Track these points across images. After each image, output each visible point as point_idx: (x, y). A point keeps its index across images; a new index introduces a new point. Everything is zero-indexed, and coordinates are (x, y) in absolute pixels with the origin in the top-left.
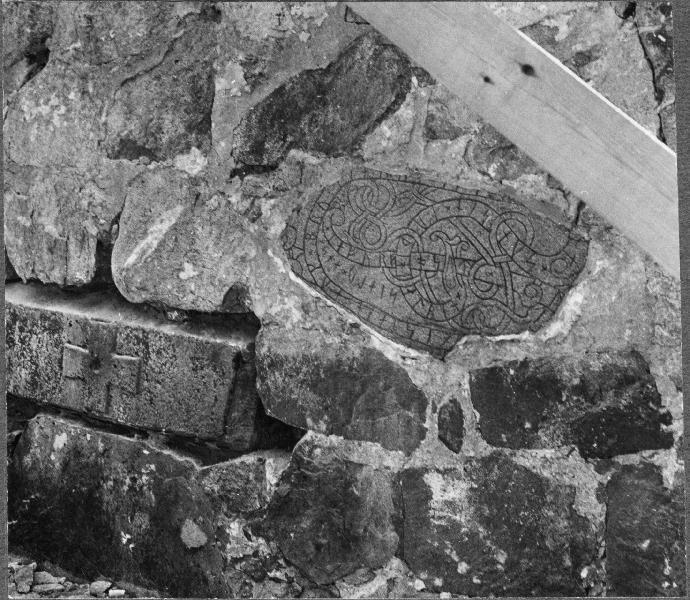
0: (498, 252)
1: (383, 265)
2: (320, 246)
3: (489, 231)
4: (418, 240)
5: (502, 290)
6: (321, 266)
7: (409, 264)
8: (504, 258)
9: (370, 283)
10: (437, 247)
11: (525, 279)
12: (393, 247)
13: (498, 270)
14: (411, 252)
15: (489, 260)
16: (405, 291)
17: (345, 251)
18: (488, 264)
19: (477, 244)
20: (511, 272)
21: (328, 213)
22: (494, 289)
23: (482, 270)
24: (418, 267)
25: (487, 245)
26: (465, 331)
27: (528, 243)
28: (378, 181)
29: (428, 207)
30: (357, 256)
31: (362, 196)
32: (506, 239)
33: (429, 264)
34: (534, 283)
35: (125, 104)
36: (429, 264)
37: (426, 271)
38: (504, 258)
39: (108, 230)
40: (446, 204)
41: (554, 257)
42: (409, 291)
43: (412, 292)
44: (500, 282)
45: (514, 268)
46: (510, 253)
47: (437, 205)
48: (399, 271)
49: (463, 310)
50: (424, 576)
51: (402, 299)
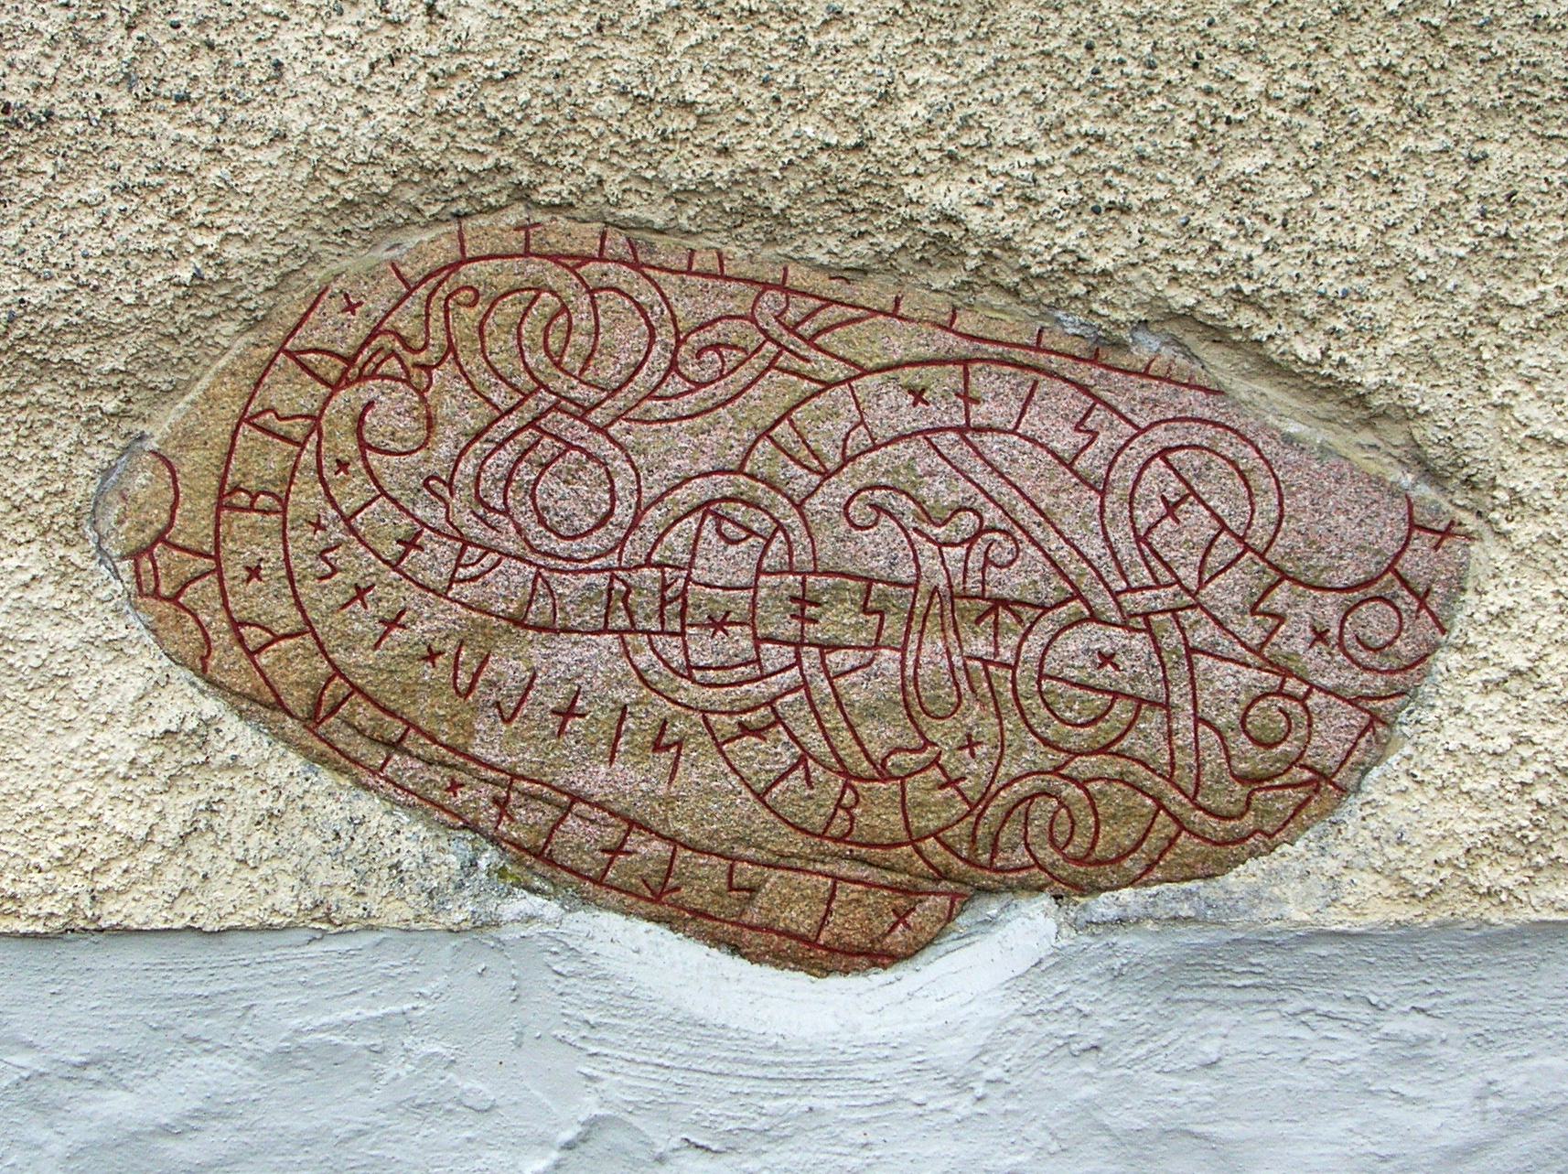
0: (1141, 575)
1: (621, 621)
3: (1103, 489)
4: (793, 520)
5: (1152, 721)
6: (308, 626)
7: (751, 621)
8: (1166, 596)
9: (558, 699)
10: (878, 548)
11: (1248, 675)
13: (1139, 643)
14: (760, 571)
15: (1102, 602)
16: (726, 724)
17: (434, 559)
18: (1094, 617)
19: (1054, 543)
20: (1191, 650)
23: (1074, 642)
24: (791, 629)
25: (1094, 548)
27: (1259, 539)
28: (592, 268)
29: (828, 385)
30: (497, 583)
33: (838, 620)
34: (1280, 692)
36: (838, 620)
38: (1166, 596)
39: (973, 407)
42: (745, 730)
43: (758, 732)
44: (1146, 689)
45: (1203, 634)
46: (1189, 576)
47: (872, 381)
48: (704, 647)
49: (987, 797)
51: (713, 763)
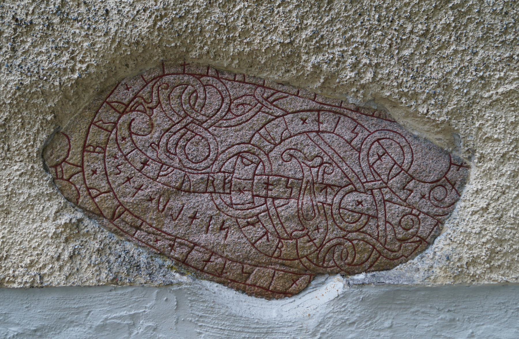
0: (370, 177)
2: (110, 162)
6: (111, 190)
10: (291, 168)
11: (402, 208)
12: (228, 166)
13: (369, 198)
21: (124, 117)
22: (363, 219)
25: (357, 169)
26: (321, 270)
27: (405, 167)
31: (180, 97)
32: (379, 162)
35: (65, 198)
37: (274, 198)
40: (300, 115)
41: (434, 184)
43: (253, 224)
47: (290, 116)
49: (322, 245)
50: (2, 39)
